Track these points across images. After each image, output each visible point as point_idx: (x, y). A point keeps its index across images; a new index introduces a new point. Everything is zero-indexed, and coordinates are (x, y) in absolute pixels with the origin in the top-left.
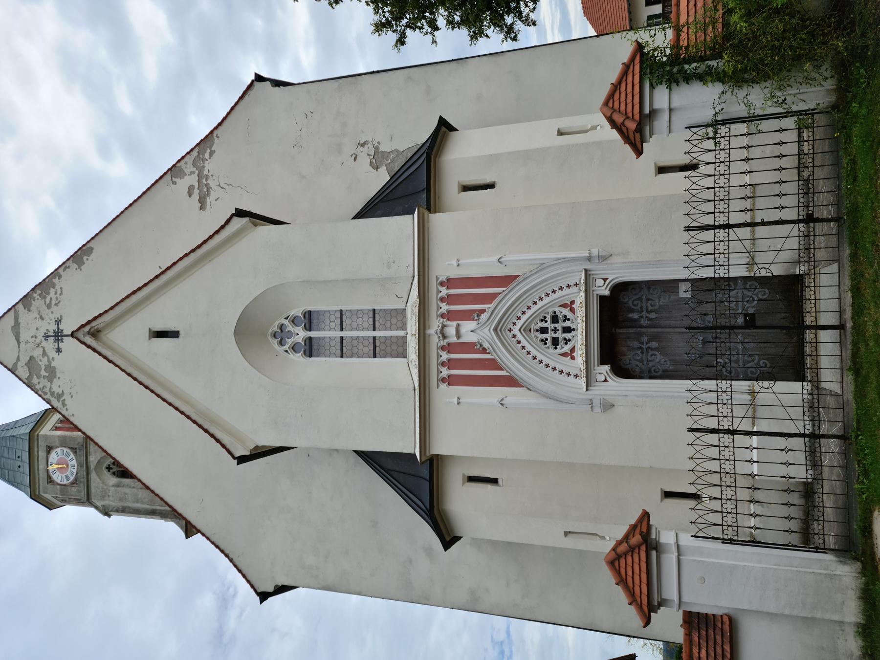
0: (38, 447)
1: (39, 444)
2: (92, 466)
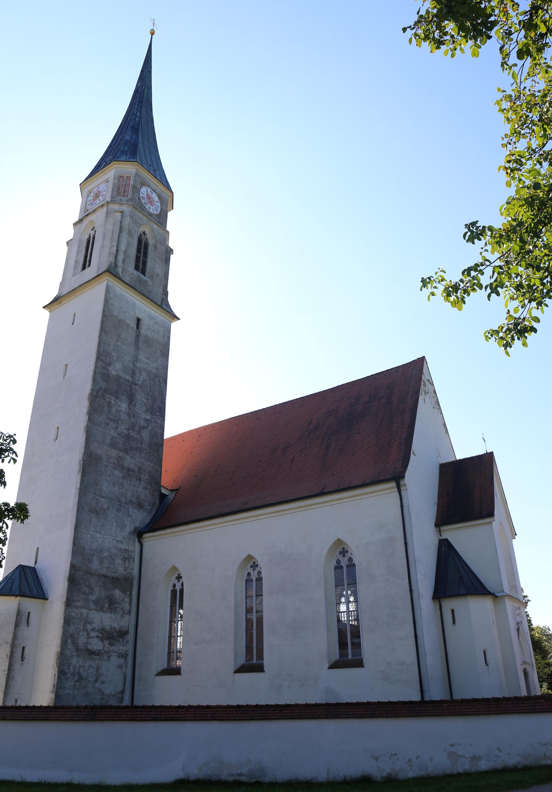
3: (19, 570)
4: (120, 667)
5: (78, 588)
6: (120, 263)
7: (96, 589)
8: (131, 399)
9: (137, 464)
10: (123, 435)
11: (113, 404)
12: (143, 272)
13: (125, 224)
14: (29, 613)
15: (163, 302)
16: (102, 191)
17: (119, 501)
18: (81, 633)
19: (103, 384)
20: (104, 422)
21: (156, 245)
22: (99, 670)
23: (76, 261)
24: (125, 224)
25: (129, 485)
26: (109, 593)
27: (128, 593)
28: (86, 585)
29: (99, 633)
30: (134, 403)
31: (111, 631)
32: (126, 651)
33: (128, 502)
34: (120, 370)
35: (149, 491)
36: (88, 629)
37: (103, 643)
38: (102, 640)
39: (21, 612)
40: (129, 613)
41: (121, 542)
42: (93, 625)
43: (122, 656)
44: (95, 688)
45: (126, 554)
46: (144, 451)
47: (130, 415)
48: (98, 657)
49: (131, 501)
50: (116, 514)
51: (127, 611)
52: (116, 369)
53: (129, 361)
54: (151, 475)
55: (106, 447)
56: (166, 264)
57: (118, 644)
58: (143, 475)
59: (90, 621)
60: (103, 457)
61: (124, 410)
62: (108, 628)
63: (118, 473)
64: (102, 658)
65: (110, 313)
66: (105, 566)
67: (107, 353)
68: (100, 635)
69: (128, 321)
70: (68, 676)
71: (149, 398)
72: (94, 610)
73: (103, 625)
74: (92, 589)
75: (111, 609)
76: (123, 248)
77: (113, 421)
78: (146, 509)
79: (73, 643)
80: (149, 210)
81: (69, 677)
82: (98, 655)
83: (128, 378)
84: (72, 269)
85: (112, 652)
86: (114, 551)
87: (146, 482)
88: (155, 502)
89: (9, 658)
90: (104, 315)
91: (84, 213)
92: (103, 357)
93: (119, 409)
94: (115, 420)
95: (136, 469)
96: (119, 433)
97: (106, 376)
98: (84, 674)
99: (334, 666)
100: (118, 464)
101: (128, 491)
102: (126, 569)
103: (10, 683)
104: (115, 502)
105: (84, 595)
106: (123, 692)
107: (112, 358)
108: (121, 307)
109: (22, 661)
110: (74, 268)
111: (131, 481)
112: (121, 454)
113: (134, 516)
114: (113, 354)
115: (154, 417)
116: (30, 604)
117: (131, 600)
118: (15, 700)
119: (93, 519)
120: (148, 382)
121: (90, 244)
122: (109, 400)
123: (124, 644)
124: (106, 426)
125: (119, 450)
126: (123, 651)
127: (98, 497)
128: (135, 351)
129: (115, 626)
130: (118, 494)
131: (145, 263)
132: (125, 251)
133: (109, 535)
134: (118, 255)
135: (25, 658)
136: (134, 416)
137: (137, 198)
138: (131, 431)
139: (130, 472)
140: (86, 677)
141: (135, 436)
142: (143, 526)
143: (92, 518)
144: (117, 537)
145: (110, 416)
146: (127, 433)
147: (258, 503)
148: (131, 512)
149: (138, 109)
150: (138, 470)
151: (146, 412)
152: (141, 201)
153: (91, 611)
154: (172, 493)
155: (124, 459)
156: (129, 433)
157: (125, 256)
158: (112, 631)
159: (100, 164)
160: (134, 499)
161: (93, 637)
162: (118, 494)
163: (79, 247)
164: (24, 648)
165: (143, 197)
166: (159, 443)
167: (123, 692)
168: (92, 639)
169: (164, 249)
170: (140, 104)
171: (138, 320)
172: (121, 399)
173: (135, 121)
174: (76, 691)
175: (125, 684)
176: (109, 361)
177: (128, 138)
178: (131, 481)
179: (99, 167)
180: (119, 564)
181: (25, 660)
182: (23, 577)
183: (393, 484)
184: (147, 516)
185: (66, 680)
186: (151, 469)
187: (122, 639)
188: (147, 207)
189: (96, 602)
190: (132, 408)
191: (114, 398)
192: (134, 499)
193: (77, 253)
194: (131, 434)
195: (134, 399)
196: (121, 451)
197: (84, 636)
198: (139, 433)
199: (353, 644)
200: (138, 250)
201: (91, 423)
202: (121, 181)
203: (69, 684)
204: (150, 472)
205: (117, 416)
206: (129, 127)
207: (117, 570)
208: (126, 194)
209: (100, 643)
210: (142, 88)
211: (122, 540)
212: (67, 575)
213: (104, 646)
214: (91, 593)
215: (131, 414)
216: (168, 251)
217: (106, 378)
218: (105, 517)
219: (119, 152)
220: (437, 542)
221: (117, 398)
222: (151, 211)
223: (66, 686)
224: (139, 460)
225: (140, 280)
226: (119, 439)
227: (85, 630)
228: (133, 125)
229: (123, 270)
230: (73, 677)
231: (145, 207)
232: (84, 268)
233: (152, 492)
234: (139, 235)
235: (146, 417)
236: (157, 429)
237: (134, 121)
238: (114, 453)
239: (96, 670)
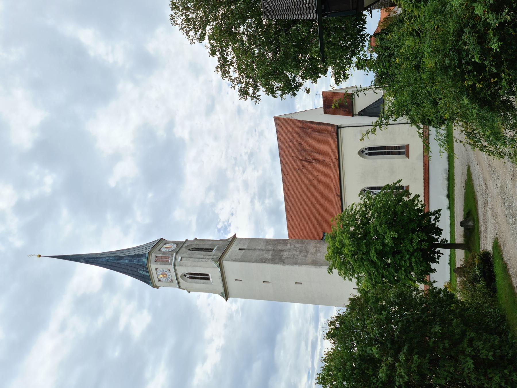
5: (457, 118)
6: (212, 257)
12: (213, 249)
19: (277, 260)
23: (204, 283)
55: (307, 258)
61: (288, 253)
76: (202, 256)
83: (271, 252)
90: (242, 261)
95: (315, 248)
99: (408, 156)
112: (309, 253)
121: (194, 276)
132: (203, 255)
147: (338, 188)
165: (168, 250)
171: (240, 249)
183: (339, 129)
193: (199, 283)
198: (298, 248)
199: (399, 149)
215: (289, 250)
220: (360, 117)
225: (218, 249)
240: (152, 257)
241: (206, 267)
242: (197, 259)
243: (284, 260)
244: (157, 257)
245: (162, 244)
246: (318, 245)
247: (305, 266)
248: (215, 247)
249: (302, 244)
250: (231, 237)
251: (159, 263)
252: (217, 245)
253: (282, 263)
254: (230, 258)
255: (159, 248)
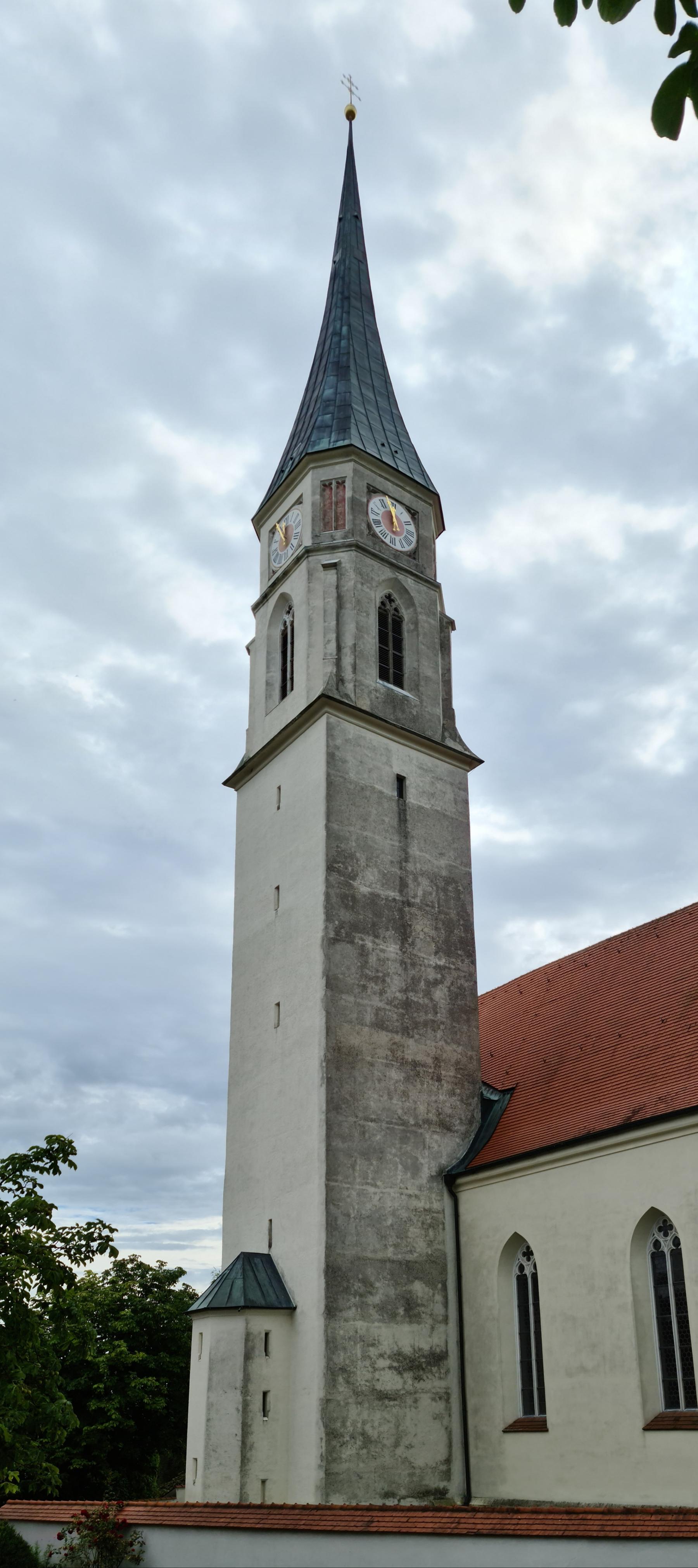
0: (416, 496)
1: (420, 501)
2: (401, 577)
3: (241, 1263)
4: (437, 1417)
6: (348, 674)
7: (377, 1285)
8: (404, 933)
9: (430, 1052)
10: (396, 1002)
11: (371, 949)
12: (399, 683)
13: (346, 588)
14: (267, 1335)
15: (446, 734)
16: (294, 525)
17: (403, 1124)
18: (359, 1362)
19: (345, 915)
20: (358, 985)
21: (417, 619)
22: (399, 1425)
24: (346, 588)
25: (419, 1092)
26: (404, 1289)
27: (440, 1286)
28: (359, 1280)
29: (394, 1361)
30: (410, 940)
31: (415, 1356)
32: (448, 1388)
33: (421, 1122)
34: (376, 883)
35: (460, 1098)
36: (372, 1356)
37: (402, 1378)
38: (400, 1373)
39: (252, 1333)
40: (446, 1320)
41: (416, 1196)
42: (380, 1347)
43: (440, 1398)
44: (396, 1456)
45: (428, 1217)
46: (442, 1027)
47: (405, 963)
48: (396, 1402)
49: (427, 1122)
50: (401, 1148)
51: (441, 1318)
52: (368, 883)
53: (392, 862)
54: (461, 1069)
55: (366, 1029)
56: (442, 654)
57: (430, 1376)
58: (444, 1070)
59: (374, 1342)
60: (364, 1049)
62: (407, 1350)
63: (395, 1074)
64: (403, 1405)
65: (341, 777)
66: (391, 1243)
67: (346, 855)
68: (395, 1364)
69: (378, 787)
70: (345, 1439)
71: (440, 925)
72: (378, 1322)
73: (398, 1346)
74: (372, 1285)
75: (410, 1317)
77: (375, 979)
78: (457, 1132)
79: (348, 1382)
80: (393, 546)
81: (347, 1441)
82: (395, 1400)
83: (393, 894)
84: (263, 700)
85: (420, 1393)
86: (404, 1214)
87: (453, 1082)
88: (473, 1116)
89: (241, 1413)
91: (269, 580)
92: (340, 865)
93: (382, 955)
94: (378, 977)
95: (429, 1061)
96: (388, 1000)
97: (350, 898)
98: (373, 1433)
99: (655, 1425)
100: (393, 1056)
101: (419, 1103)
102: (430, 1243)
103: (248, 1455)
104: (396, 1127)
105: (357, 1298)
106: (448, 1461)
107: (357, 863)
108: (361, 762)
109: (264, 1416)
110: (266, 698)
111: (422, 1084)
112: (398, 1038)
113: (436, 1147)
114: (358, 855)
115: (454, 960)
116: (261, 1322)
117: (446, 1298)
118: (260, 1482)
119: (359, 1162)
120: (434, 896)
122: (361, 942)
123: (442, 1376)
124: (363, 992)
125: (391, 1031)
126: (440, 1388)
127: (362, 1122)
128: (400, 842)
129: (421, 1346)
130: (400, 1112)
131: (399, 663)
132: (355, 645)
133: (391, 1187)
134: (342, 658)
135: (269, 1411)
136: (413, 965)
137: (364, 526)
138: (411, 994)
139: (418, 1069)
140: (378, 1440)
141: (421, 1001)
142: (454, 1162)
143: (355, 1160)
144: (407, 1189)
145: (367, 971)
146: (405, 998)
148: (428, 1140)
149: (341, 319)
150: (433, 1063)
151: (436, 953)
152: (374, 531)
153: (373, 1323)
154: (504, 1095)
155: (404, 1047)
156: (407, 998)
157: (355, 656)
158: (417, 1355)
159: (283, 467)
160: (432, 1116)
161: (384, 1369)
162: (400, 1112)
163: (268, 653)
164: (265, 1394)
165: (378, 522)
166: (469, 1007)
167: (448, 1461)
168: (382, 1372)
169: (435, 623)
170: (346, 304)
171: (401, 780)
172: (384, 937)
173: (340, 347)
174: (361, 1465)
175: (450, 1446)
176: (353, 870)
177: (328, 393)
178: (422, 1084)
179: (282, 474)
180: (417, 1237)
181: (270, 1414)
182: (250, 1274)
184: (461, 1143)
185: (341, 1446)
186: (459, 1056)
187: (436, 1368)
188: (387, 541)
189: (381, 1308)
190: (409, 950)
191: (371, 938)
192: (432, 1116)
193: (268, 667)
194: (413, 998)
195: (411, 932)
196: (397, 1032)
197: (366, 1367)
198: (428, 994)
200: (383, 637)
201: (332, 990)
202: (327, 496)
203: (349, 1452)
204: (457, 1063)
205: (380, 969)
206: (330, 366)
207: (413, 1247)
208: (341, 522)
209: (397, 1378)
210: (345, 264)
211: (417, 1192)
212: (323, 1266)
213: (405, 1383)
214: (371, 1293)
215: (408, 962)
216: (445, 624)
217: (351, 904)
218: (381, 1156)
219: (315, 431)
221: (377, 936)
222: (398, 547)
223: (344, 1456)
224: (433, 1044)
225: (392, 700)
226: (390, 1010)
227: (365, 1357)
228: (336, 360)
229: (355, 686)
230: (353, 1440)
231: (383, 542)
232: (284, 694)
233: (464, 1098)
234: (378, 604)
235: (439, 963)
236: (462, 981)
237: (337, 349)
238: (383, 1038)
239: (395, 1425)
240: (337, 467)
241: (308, 667)
242: (334, 623)
243: (352, 942)
244: (341, 483)
245: (407, 498)
246: (448, 1073)
247: (324, 1020)
248: (409, 691)
249: (451, 1012)
250: (467, 749)
251: (318, 497)
252: (419, 697)
253: (332, 935)
254: (347, 741)
255: (379, 482)
